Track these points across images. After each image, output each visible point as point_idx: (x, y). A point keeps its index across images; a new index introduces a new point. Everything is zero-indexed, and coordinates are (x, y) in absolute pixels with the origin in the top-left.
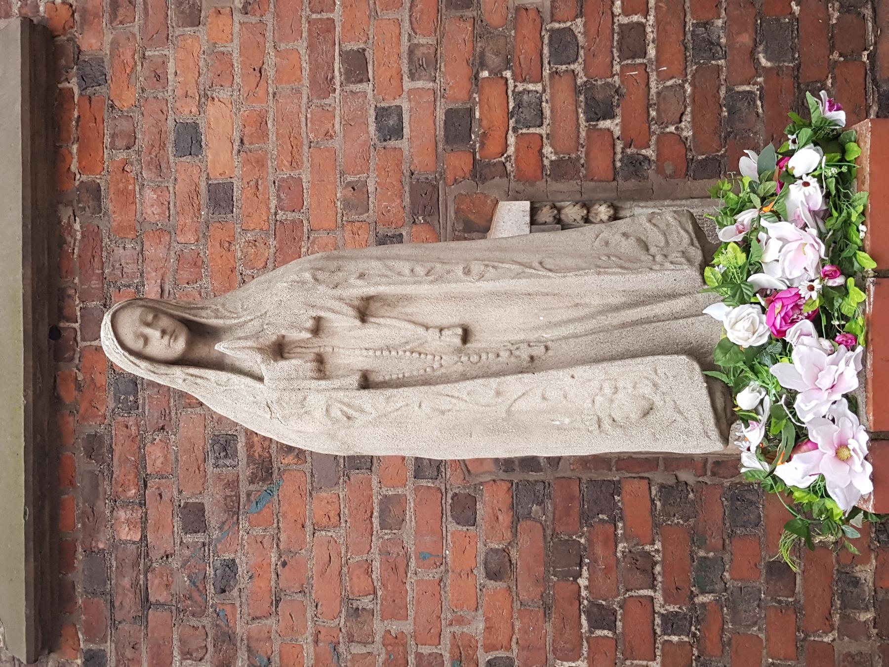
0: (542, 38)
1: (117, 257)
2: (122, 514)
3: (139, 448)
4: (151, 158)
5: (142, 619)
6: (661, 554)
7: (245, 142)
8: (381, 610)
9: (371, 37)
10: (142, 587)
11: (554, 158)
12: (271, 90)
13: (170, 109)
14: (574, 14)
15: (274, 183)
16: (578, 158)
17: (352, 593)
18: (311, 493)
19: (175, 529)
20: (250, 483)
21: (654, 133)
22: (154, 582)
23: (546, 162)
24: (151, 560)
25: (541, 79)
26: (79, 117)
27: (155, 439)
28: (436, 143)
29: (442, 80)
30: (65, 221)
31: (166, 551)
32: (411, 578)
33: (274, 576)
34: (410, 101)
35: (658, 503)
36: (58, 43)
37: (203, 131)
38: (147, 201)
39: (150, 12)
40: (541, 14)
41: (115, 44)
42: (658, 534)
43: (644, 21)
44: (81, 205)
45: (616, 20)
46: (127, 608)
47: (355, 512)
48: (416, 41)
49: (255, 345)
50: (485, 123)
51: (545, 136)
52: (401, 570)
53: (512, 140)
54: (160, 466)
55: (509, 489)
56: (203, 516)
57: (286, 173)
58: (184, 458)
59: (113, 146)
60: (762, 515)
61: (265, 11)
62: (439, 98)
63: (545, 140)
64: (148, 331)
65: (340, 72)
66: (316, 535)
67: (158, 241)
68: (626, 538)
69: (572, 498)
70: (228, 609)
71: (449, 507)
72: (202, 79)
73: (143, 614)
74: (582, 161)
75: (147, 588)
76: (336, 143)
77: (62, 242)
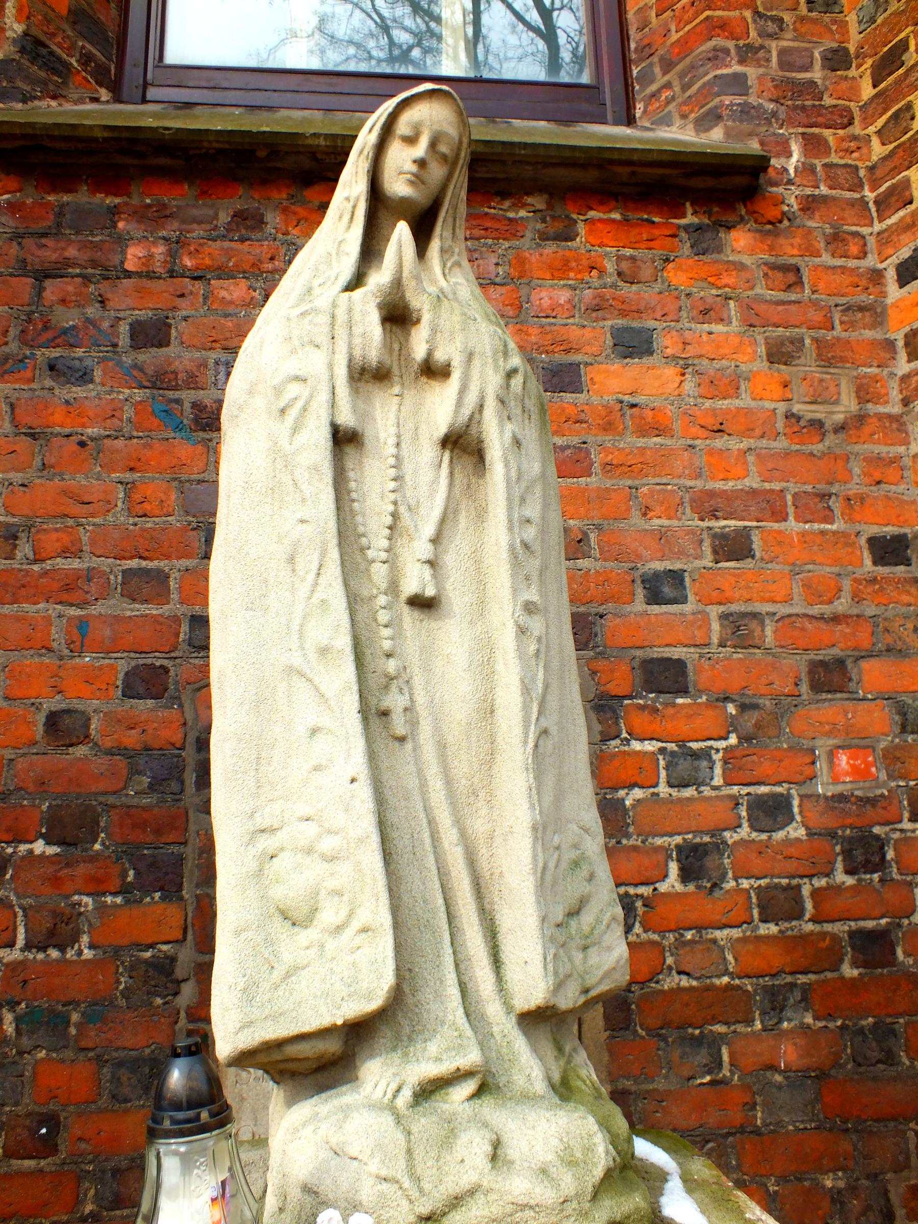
0: (779, 783)
1: (486, 255)
2: (160, 250)
3: (244, 272)
4: (608, 300)
5: (23, 268)
6: (75, 958)
7: (634, 410)
8: (13, 569)
9: (770, 566)
10: (63, 271)
11: (628, 803)
12: (698, 442)
13: (668, 324)
14: (811, 824)
15: (584, 443)
16: (628, 836)
17: (38, 532)
18: (175, 479)
19: (137, 312)
20: (193, 403)
21: (663, 937)
22: (70, 287)
23: (622, 793)
24: (98, 282)
25: (728, 783)
26: (653, 223)
27: (255, 291)
28: (643, 647)
29: (722, 655)
30: (530, 200)
31: (108, 300)
32: (55, 609)
33: (67, 431)
34: (693, 614)
35: (148, 954)
36: (737, 206)
37: (644, 360)
38: (556, 292)
39: (780, 308)
40: (808, 782)
41: (740, 267)
42: (105, 953)
43: (807, 916)
44: (548, 219)
45: (806, 880)
46: (39, 253)
47: (148, 536)
48: (767, 621)
49: (405, 274)
50: (671, 711)
51: (655, 790)
52: (65, 597)
53: (650, 746)
54: (220, 296)
55: (173, 744)
56: (153, 346)
57: (597, 458)
58: (230, 324)
59: (620, 258)
60: (129, 1104)
61: (791, 440)
62: (699, 651)
63: (652, 790)
64: (424, 142)
65: (724, 527)
66: (119, 485)
67: (507, 302)
68: (101, 908)
69: (158, 832)
70: (29, 374)
71: (149, 661)
72: (705, 362)
73: (29, 271)
74: (624, 841)
75: (62, 277)
76: (636, 519)
77: (504, 195)
